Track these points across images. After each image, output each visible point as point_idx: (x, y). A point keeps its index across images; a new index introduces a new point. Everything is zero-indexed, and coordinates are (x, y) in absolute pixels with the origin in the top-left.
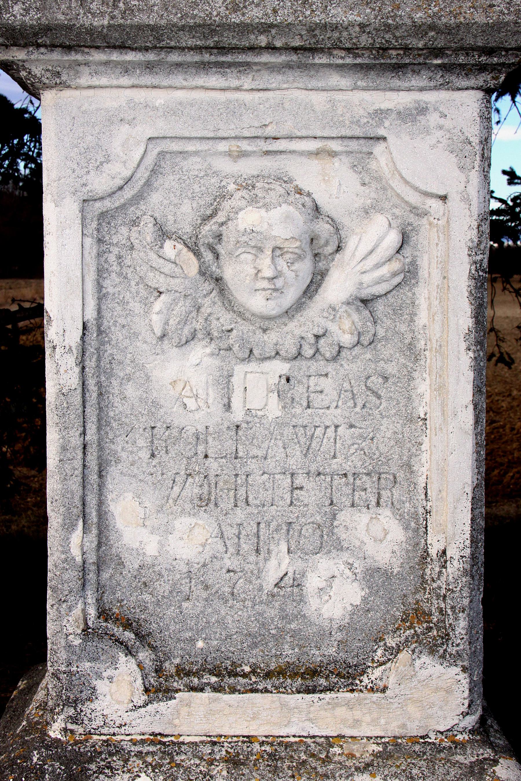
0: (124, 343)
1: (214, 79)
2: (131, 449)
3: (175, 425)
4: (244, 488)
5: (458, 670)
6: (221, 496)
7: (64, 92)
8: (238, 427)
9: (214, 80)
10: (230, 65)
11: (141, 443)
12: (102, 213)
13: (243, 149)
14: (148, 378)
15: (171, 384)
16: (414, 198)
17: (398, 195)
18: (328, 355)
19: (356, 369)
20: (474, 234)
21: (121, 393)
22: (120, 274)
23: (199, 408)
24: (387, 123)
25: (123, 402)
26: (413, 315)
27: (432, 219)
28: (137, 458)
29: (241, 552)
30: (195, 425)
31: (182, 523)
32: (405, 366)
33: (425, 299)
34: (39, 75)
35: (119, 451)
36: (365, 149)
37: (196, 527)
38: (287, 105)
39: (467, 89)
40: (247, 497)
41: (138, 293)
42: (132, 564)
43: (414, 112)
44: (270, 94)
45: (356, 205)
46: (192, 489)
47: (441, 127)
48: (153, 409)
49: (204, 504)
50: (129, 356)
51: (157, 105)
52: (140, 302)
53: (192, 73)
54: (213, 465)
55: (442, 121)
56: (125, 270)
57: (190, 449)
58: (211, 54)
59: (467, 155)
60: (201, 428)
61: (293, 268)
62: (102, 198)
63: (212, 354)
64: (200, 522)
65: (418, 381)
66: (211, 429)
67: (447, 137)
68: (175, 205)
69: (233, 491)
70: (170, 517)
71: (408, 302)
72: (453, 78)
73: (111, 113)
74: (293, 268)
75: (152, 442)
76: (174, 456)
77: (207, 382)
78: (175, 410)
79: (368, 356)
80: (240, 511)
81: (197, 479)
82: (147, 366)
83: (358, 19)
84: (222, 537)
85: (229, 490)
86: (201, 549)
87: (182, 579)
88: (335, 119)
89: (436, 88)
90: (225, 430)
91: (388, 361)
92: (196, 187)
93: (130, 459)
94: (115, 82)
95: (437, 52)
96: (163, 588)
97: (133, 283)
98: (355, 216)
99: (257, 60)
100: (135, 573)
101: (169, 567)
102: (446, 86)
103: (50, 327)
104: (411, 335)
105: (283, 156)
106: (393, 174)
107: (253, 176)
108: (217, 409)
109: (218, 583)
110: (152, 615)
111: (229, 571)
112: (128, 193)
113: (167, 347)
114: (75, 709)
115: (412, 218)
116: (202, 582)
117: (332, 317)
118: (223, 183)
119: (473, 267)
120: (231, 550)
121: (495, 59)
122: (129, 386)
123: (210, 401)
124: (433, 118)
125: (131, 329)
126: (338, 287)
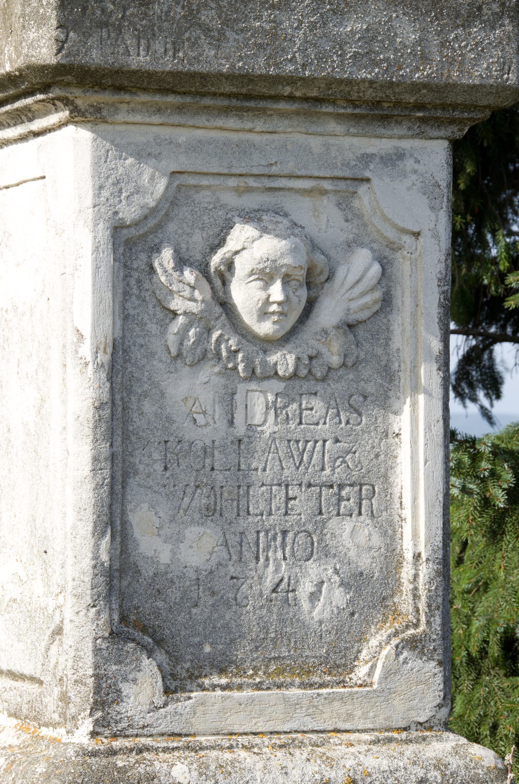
0: (142, 362)
1: (232, 121)
2: (147, 462)
3: (186, 439)
4: (246, 499)
5: (433, 664)
6: (226, 506)
7: (99, 126)
8: (240, 441)
9: (232, 122)
10: (249, 110)
11: (156, 456)
12: (127, 240)
13: (250, 185)
14: (163, 395)
15: (182, 400)
16: (391, 234)
17: (378, 231)
18: (319, 375)
19: (341, 388)
20: (442, 267)
21: (139, 409)
22: (139, 297)
23: (207, 425)
24: (372, 167)
25: (141, 417)
26: (388, 339)
27: (405, 253)
28: (152, 471)
29: (243, 560)
30: (203, 439)
31: (192, 532)
32: (382, 386)
33: (399, 325)
34: (83, 110)
35: (137, 463)
36: (351, 189)
37: (205, 535)
38: (289, 147)
39: (437, 138)
40: (248, 507)
41: (155, 315)
42: (148, 572)
43: (394, 157)
44: (276, 137)
45: (341, 239)
46: (201, 500)
47: (415, 172)
48: (167, 425)
49: (211, 514)
50: (146, 374)
51: (180, 142)
52: (157, 323)
53: (214, 114)
54: (219, 477)
55: (416, 166)
56: (143, 294)
57: (199, 462)
58: (238, 100)
59: (436, 196)
60: (208, 442)
61: (297, 294)
62: (129, 226)
63: (220, 373)
64: (208, 531)
65: (392, 399)
66: (217, 443)
67: (421, 180)
68: (188, 234)
69: (236, 502)
70: (181, 527)
71: (383, 328)
72: (428, 128)
73: (140, 148)
74: (297, 294)
75: (166, 455)
76: (185, 468)
77: (214, 399)
78: (186, 425)
79: (351, 376)
80: (242, 521)
81: (205, 490)
82: (162, 383)
83: (369, 76)
84: (227, 545)
85: (232, 500)
86: (208, 557)
87: (192, 586)
88: (329, 161)
89: (412, 137)
90: (229, 444)
91: (367, 381)
92: (206, 218)
93: (147, 471)
94: (148, 120)
95: (420, 107)
96: (174, 595)
97: (151, 306)
98: (340, 249)
99: (275, 106)
100: (150, 581)
101: (180, 574)
102: (421, 135)
103: (81, 345)
104: (386, 358)
105: (281, 193)
106: (375, 212)
107: (254, 210)
108: (222, 424)
109: (223, 589)
110: (165, 621)
111: (232, 578)
112: (152, 223)
113: (180, 366)
114: (103, 711)
115: (387, 252)
116: (209, 588)
117: (324, 340)
118: (229, 216)
119: (442, 297)
120: (235, 557)
121: (466, 114)
122: (146, 402)
123: (217, 417)
124: (409, 164)
125: (148, 348)
126: (329, 312)
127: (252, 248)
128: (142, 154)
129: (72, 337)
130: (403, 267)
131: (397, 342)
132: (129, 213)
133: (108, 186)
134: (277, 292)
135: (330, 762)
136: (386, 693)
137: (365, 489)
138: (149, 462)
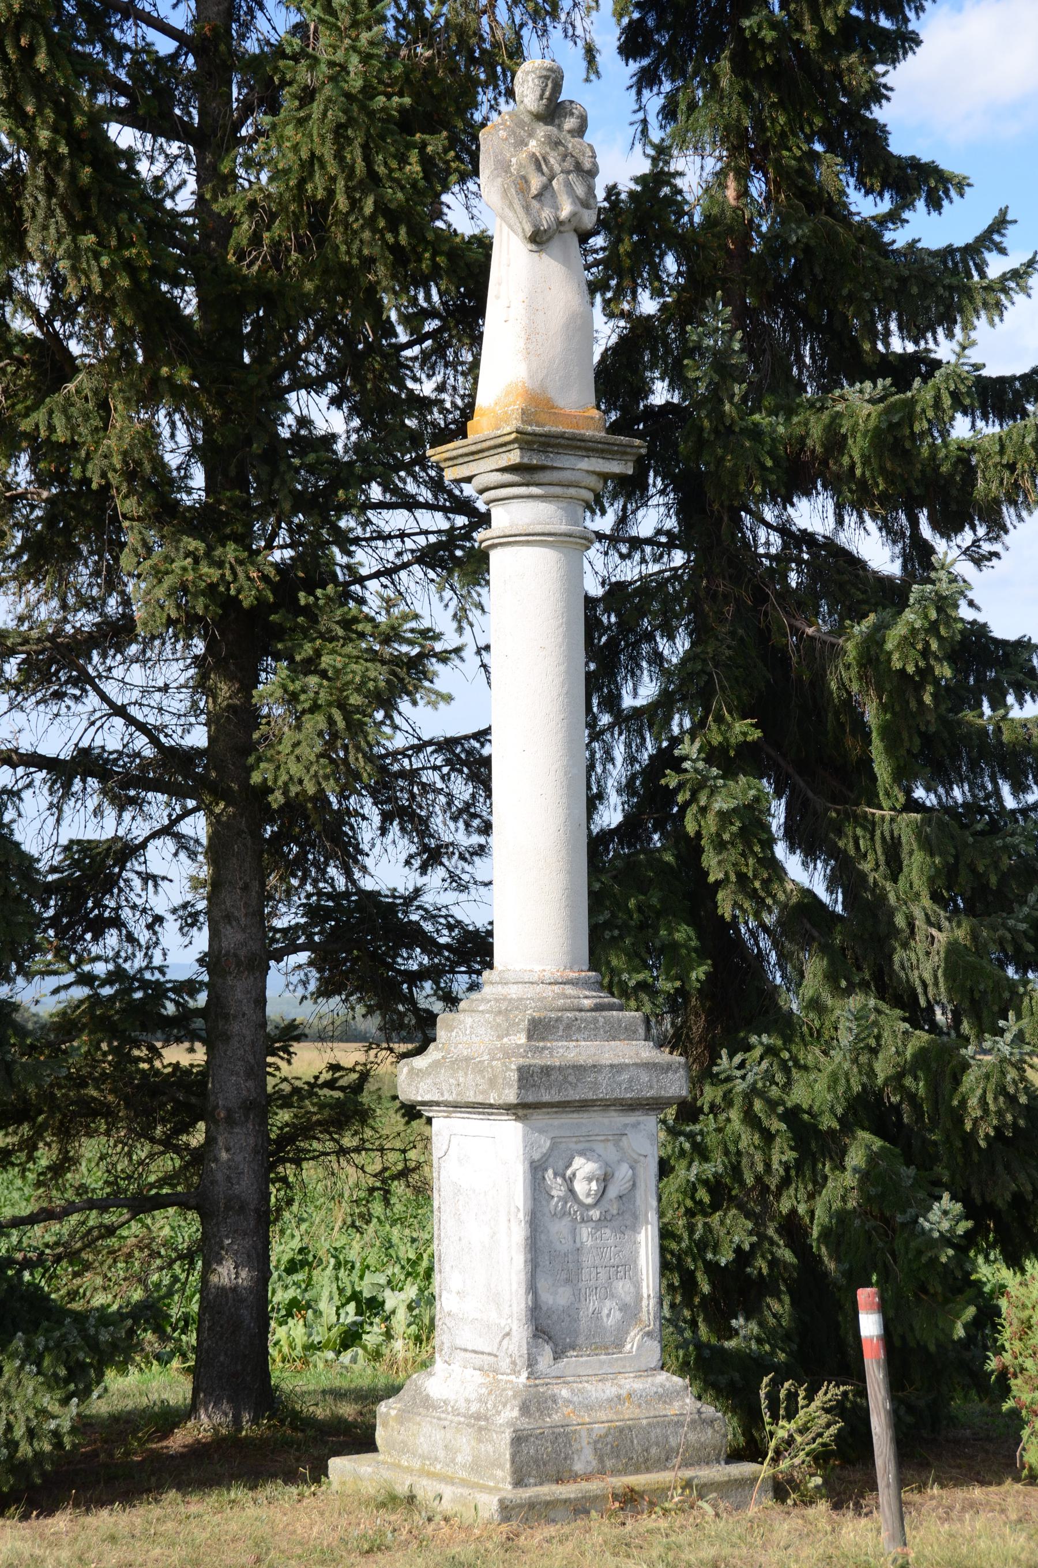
31: (561, 1290)
46: (564, 1276)
96: (555, 1317)
126: (612, 1192)
127: (583, 1168)
128: (541, 1131)
129: (513, 1210)
130: (640, 1171)
131: (638, 1202)
132: (537, 1156)
133: (529, 1145)
134: (594, 1186)
135: (620, 1387)
136: (638, 1356)
137: (627, 1267)
138: (544, 1260)
